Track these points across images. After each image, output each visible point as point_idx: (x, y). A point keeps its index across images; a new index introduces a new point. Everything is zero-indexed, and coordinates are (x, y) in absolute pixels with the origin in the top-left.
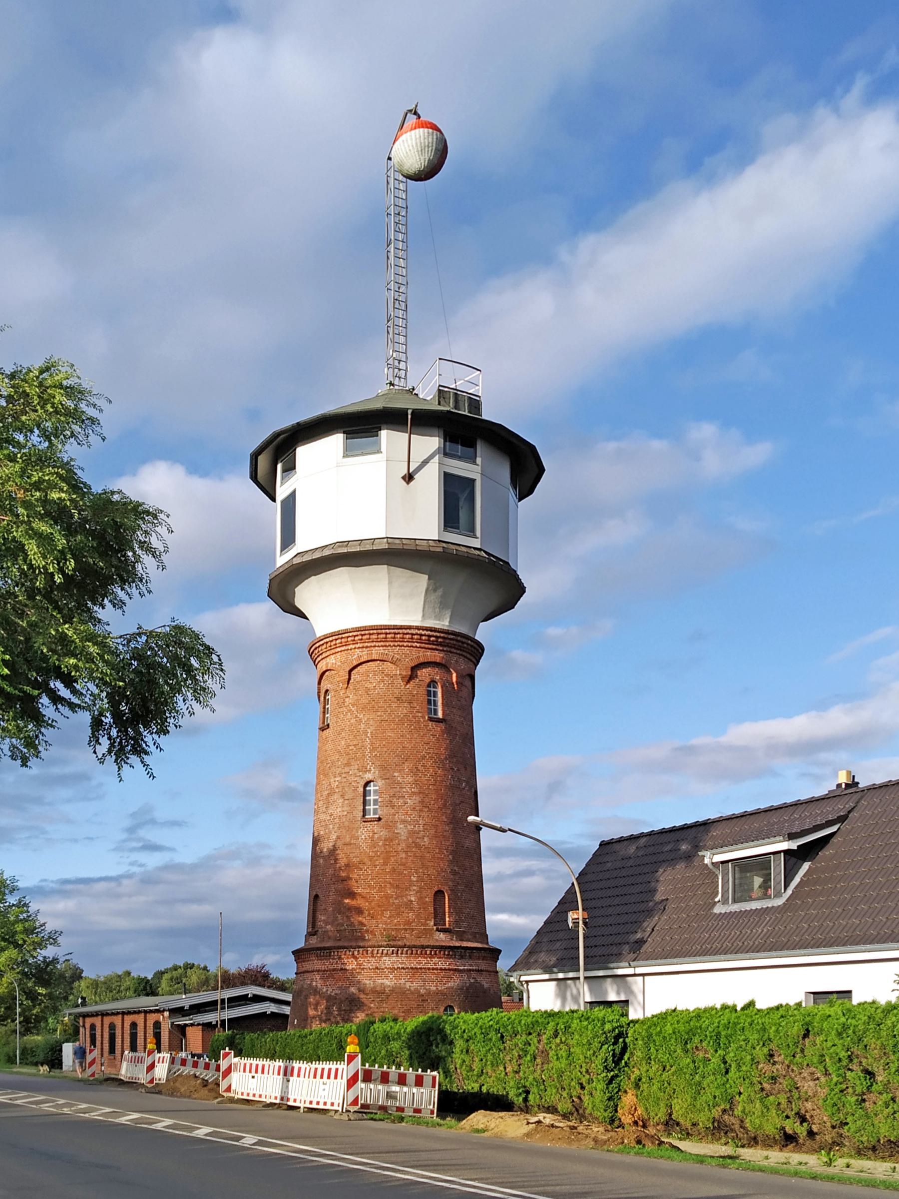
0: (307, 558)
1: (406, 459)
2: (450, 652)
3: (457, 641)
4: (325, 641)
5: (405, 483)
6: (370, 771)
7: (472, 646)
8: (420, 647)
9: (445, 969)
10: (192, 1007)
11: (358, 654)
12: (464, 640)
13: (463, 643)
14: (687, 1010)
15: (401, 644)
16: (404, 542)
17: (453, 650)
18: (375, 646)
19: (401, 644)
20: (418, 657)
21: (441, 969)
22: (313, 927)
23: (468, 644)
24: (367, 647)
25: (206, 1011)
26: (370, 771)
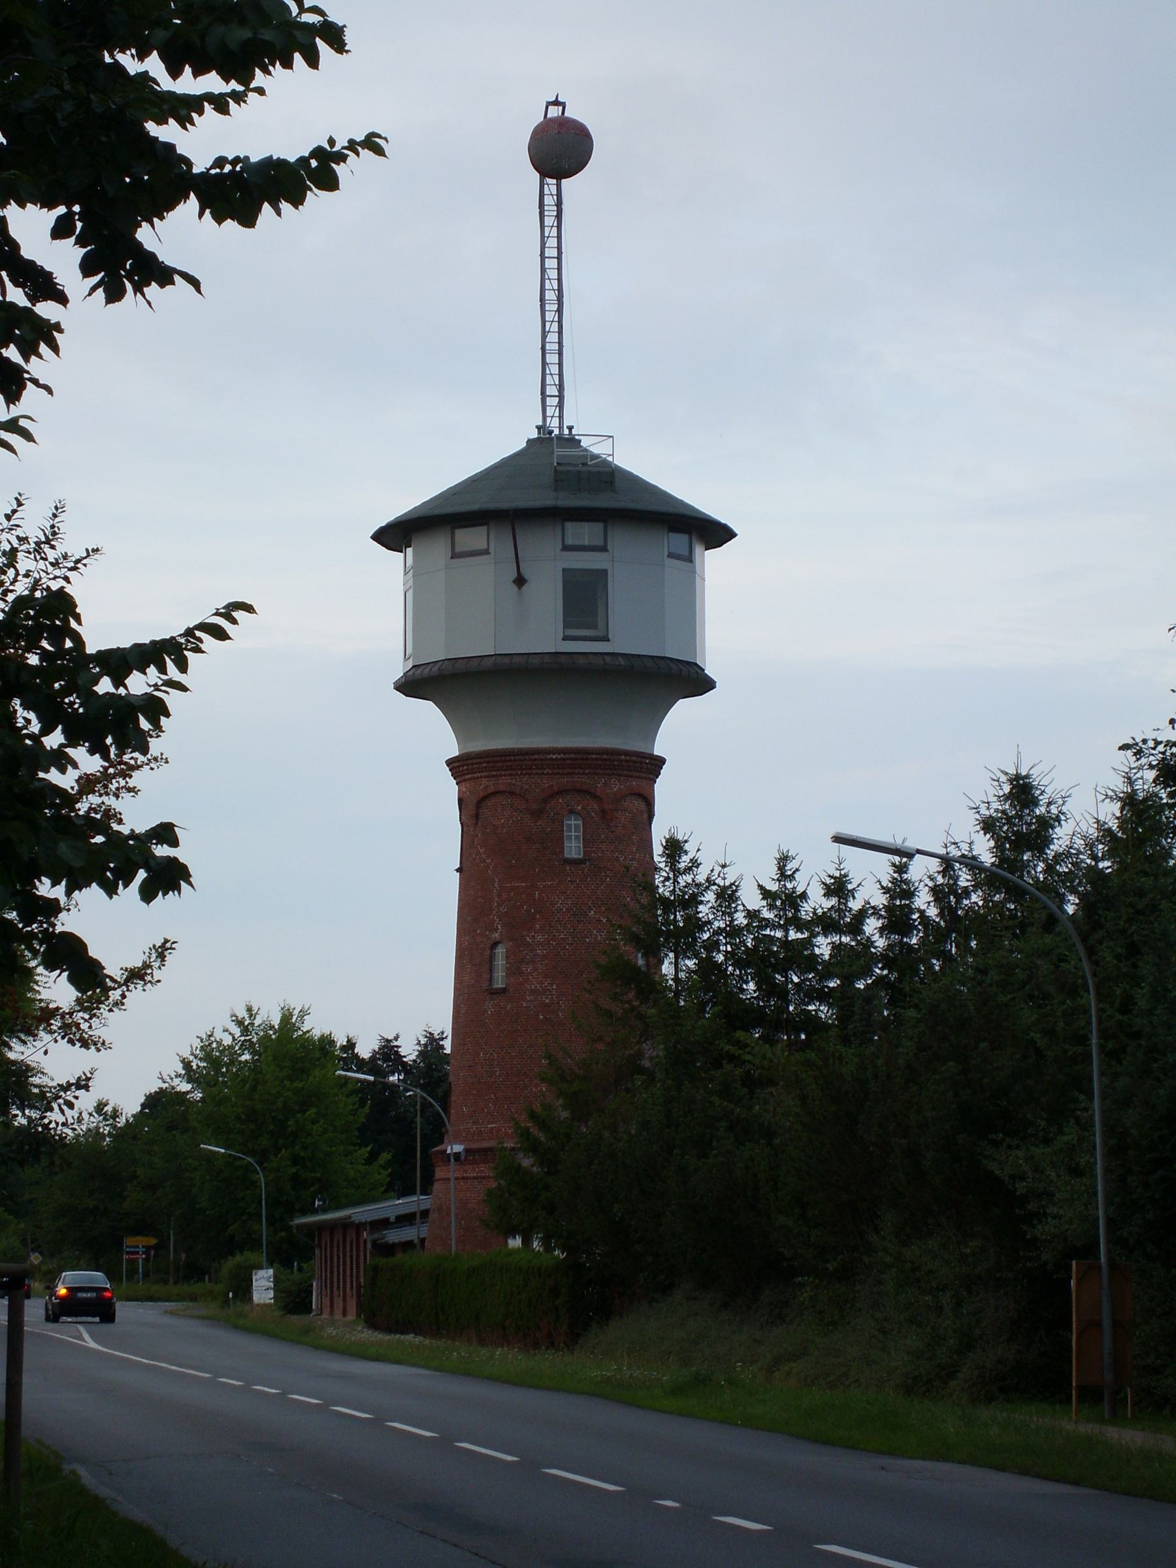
5: (515, 588)
18: (501, 775)
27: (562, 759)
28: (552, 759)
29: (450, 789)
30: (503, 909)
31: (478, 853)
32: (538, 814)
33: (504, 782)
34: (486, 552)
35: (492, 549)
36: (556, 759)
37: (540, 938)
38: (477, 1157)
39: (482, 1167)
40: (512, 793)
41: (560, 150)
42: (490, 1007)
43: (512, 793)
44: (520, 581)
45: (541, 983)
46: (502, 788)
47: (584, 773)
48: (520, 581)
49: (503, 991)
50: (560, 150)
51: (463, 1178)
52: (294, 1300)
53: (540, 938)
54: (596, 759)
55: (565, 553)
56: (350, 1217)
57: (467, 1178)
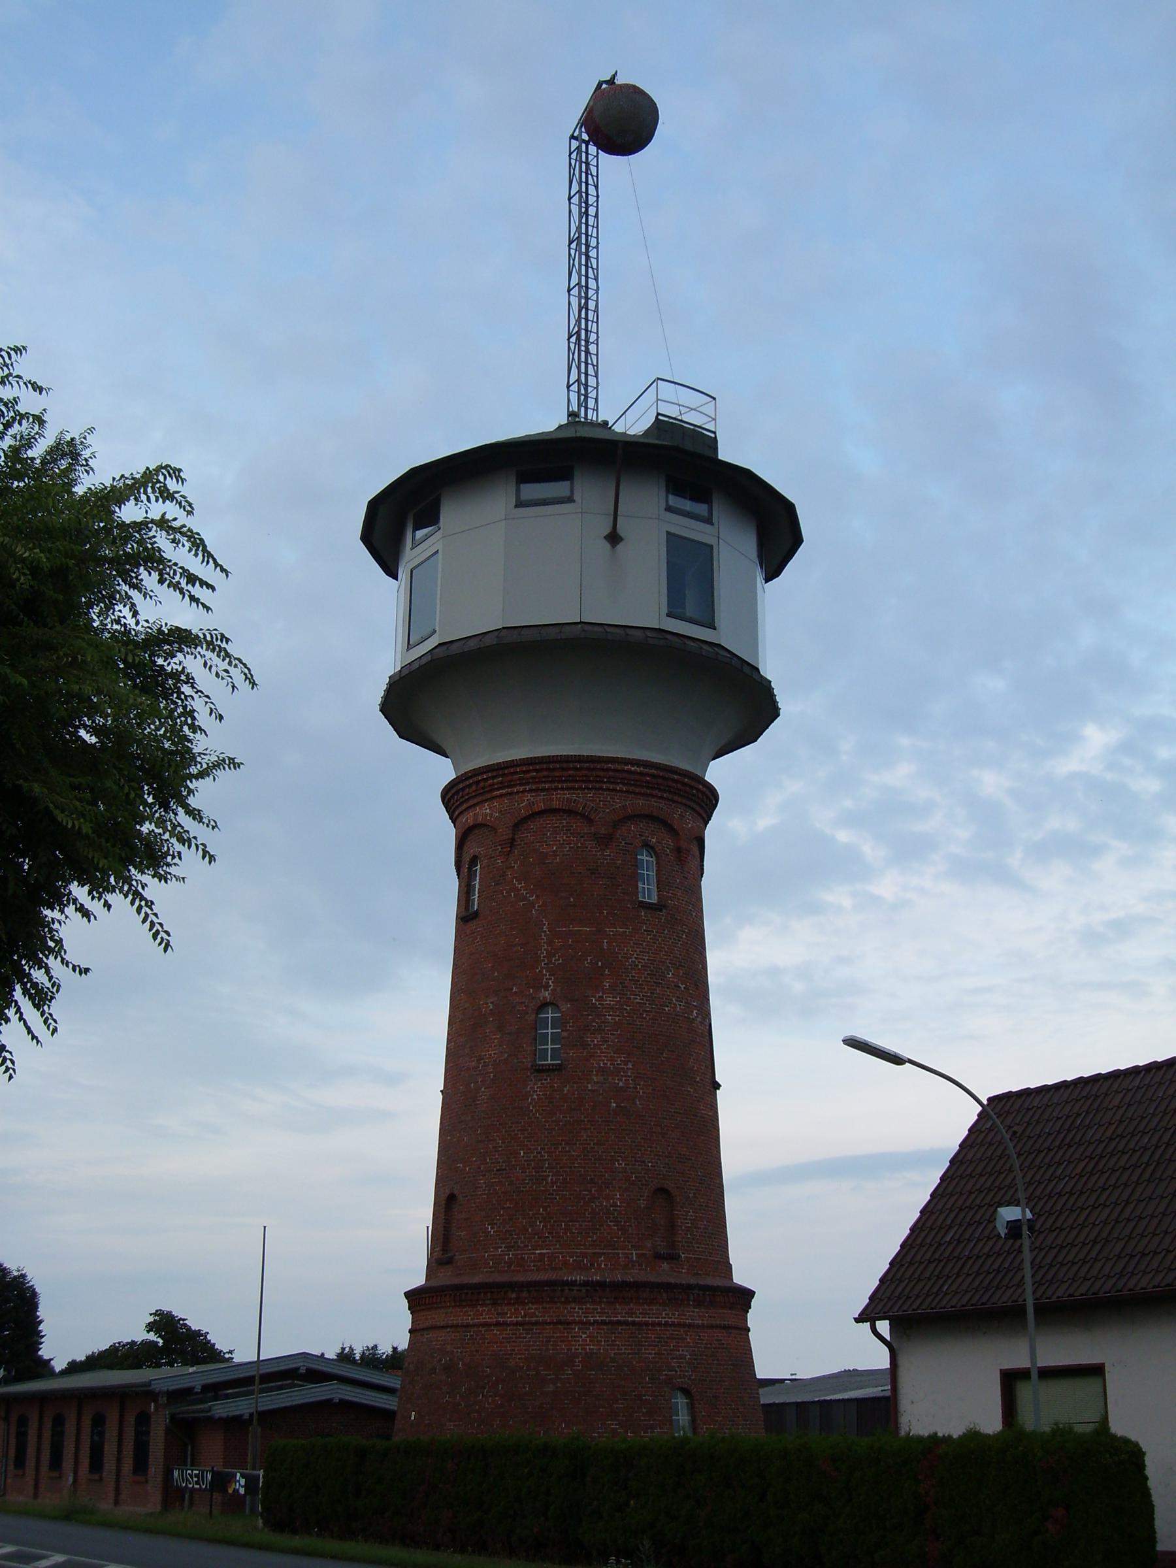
0: (454, 649)
1: (612, 512)
2: (674, 801)
3: (684, 784)
4: (475, 779)
5: (608, 546)
6: (546, 987)
7: (703, 793)
8: (627, 792)
9: (673, 1324)
10: (206, 1388)
11: (527, 801)
12: (693, 783)
13: (692, 788)
14: (133, 1342)
15: (598, 785)
16: (609, 629)
17: (676, 798)
18: (556, 789)
19: (598, 785)
20: (624, 807)
21: (666, 1324)
22: (445, 1249)
23: (698, 790)
24: (543, 790)
25: (227, 1397)
26: (546, 987)
27: (641, 774)
28: (629, 772)
29: (445, 833)
30: (557, 960)
31: (515, 889)
32: (605, 840)
33: (559, 798)
34: (570, 500)
35: (577, 497)
36: (635, 773)
37: (609, 1000)
38: (525, 1294)
39: (532, 1308)
40: (570, 812)
41: (620, 122)
42: (535, 1089)
43: (570, 812)
44: (614, 538)
45: (612, 1059)
46: (556, 804)
47: (662, 797)
48: (614, 538)
49: (558, 1068)
50: (620, 122)
51: (498, 1324)
52: (473, 1552)
53: (609, 1000)
54: (677, 781)
55: (669, 515)
56: (149, 1383)
57: (505, 1324)
